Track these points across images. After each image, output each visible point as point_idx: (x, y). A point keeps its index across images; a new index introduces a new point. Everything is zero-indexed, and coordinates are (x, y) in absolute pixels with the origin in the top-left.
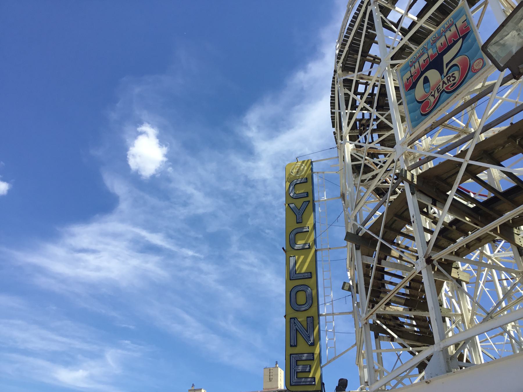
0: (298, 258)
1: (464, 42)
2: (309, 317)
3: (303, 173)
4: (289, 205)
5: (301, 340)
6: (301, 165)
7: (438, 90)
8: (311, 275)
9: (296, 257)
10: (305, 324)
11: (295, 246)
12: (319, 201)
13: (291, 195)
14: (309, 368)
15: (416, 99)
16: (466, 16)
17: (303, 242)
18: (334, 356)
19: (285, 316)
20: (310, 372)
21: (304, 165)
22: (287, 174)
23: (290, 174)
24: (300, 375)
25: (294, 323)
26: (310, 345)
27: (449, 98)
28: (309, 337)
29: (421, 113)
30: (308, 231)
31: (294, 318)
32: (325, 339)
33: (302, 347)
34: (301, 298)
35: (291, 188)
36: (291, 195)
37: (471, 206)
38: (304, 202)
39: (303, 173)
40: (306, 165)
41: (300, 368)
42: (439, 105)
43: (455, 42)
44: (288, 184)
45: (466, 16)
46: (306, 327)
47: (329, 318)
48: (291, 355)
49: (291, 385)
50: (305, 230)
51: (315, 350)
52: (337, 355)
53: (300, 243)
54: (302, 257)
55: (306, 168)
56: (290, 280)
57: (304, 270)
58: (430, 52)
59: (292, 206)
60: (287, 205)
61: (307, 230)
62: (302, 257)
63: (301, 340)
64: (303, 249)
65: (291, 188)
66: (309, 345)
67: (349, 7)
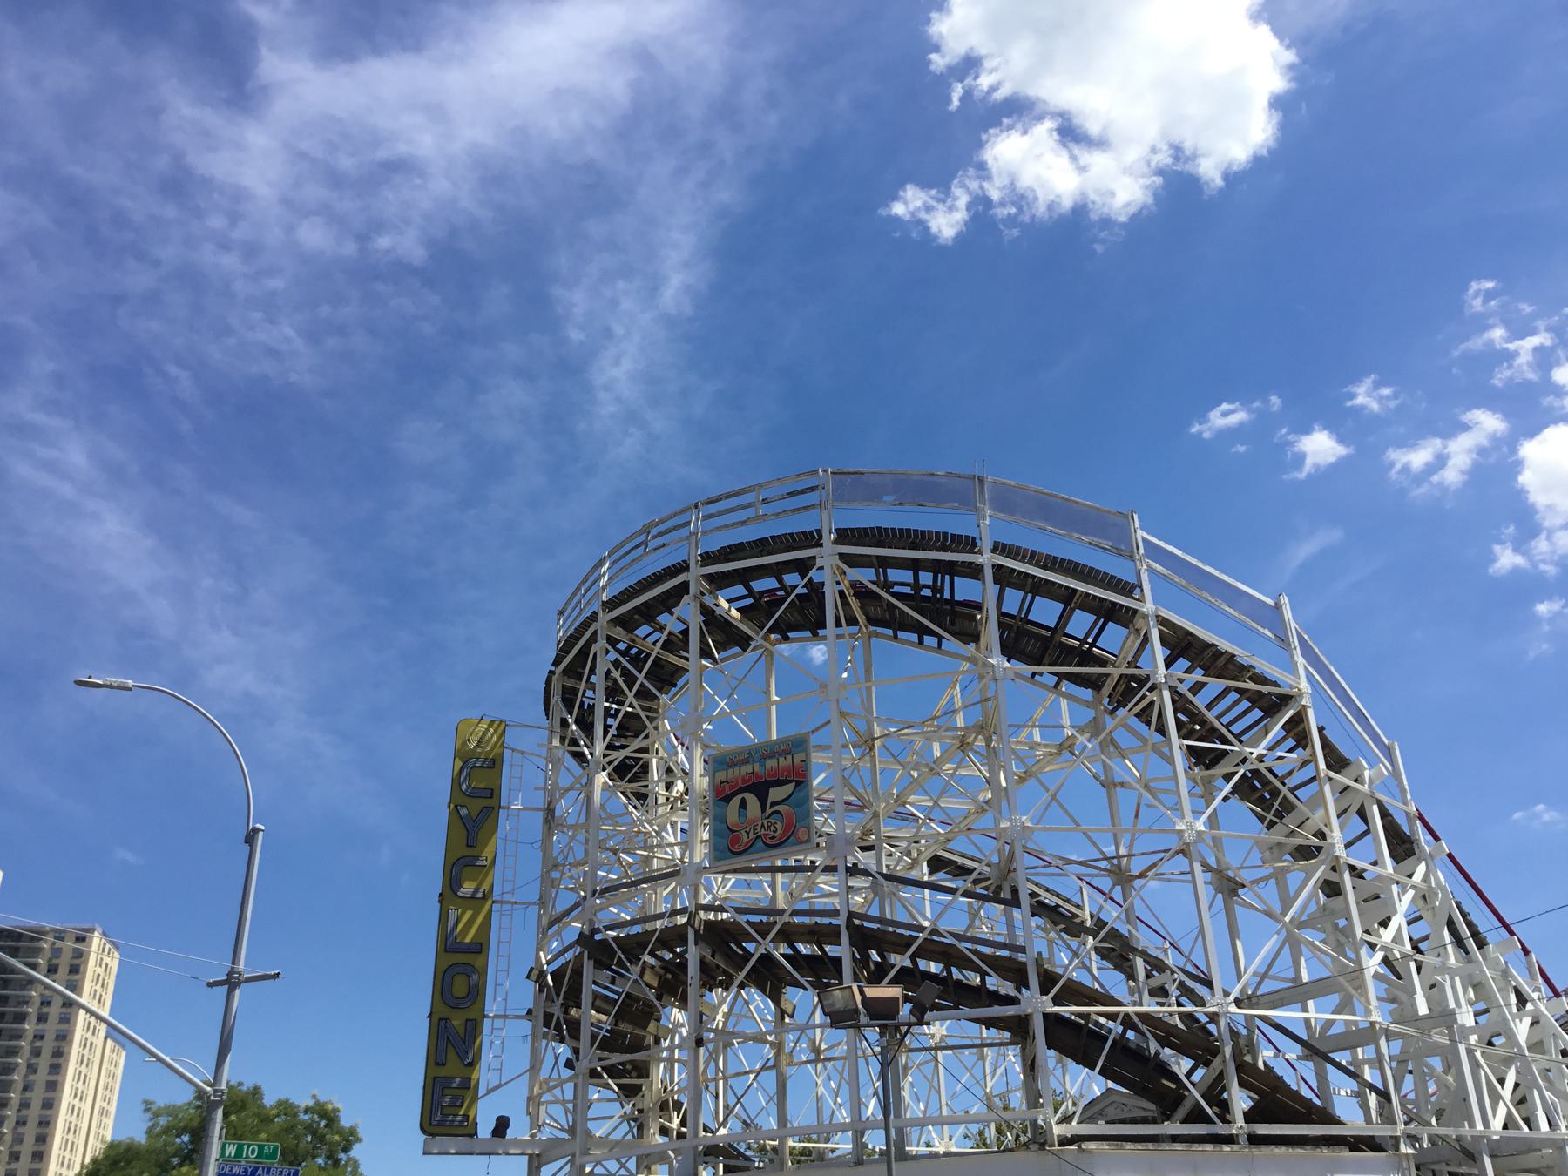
0: (463, 913)
1: (797, 790)
2: (470, 1020)
3: (488, 748)
4: (456, 806)
5: (452, 1055)
6: (487, 730)
7: (754, 830)
8: (479, 948)
9: (460, 910)
10: (461, 1030)
11: (458, 890)
12: (508, 808)
13: (464, 787)
14: (460, 1101)
15: (728, 827)
16: (806, 756)
17: (473, 885)
18: (498, 1083)
19: (429, 1016)
20: (461, 1106)
21: (492, 730)
22: (459, 743)
23: (464, 744)
24: (446, 1111)
25: (446, 1027)
26: (466, 1065)
27: (764, 851)
28: (467, 1053)
29: (729, 848)
30: (485, 866)
31: (446, 1020)
32: (487, 1057)
33: (453, 1067)
34: (460, 987)
35: (464, 774)
36: (464, 787)
37: (741, 952)
38: (484, 807)
39: (488, 748)
40: (495, 731)
41: (448, 1099)
42: (751, 853)
43: (787, 782)
44: (459, 764)
45: (806, 756)
46: (462, 1036)
47: (498, 1023)
48: (435, 1078)
49: (430, 1124)
50: (480, 863)
51: (472, 1073)
52: (502, 1083)
53: (467, 888)
54: (469, 914)
55: (494, 739)
56: (446, 951)
57: (468, 940)
58: (757, 767)
59: (464, 812)
60: (452, 806)
61: (484, 863)
62: (469, 914)
63: (452, 1055)
64: (473, 897)
65: (464, 774)
66: (466, 1065)
67: (744, 999)
